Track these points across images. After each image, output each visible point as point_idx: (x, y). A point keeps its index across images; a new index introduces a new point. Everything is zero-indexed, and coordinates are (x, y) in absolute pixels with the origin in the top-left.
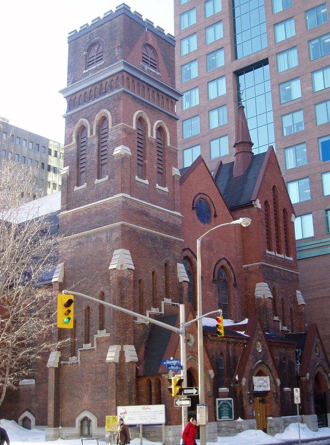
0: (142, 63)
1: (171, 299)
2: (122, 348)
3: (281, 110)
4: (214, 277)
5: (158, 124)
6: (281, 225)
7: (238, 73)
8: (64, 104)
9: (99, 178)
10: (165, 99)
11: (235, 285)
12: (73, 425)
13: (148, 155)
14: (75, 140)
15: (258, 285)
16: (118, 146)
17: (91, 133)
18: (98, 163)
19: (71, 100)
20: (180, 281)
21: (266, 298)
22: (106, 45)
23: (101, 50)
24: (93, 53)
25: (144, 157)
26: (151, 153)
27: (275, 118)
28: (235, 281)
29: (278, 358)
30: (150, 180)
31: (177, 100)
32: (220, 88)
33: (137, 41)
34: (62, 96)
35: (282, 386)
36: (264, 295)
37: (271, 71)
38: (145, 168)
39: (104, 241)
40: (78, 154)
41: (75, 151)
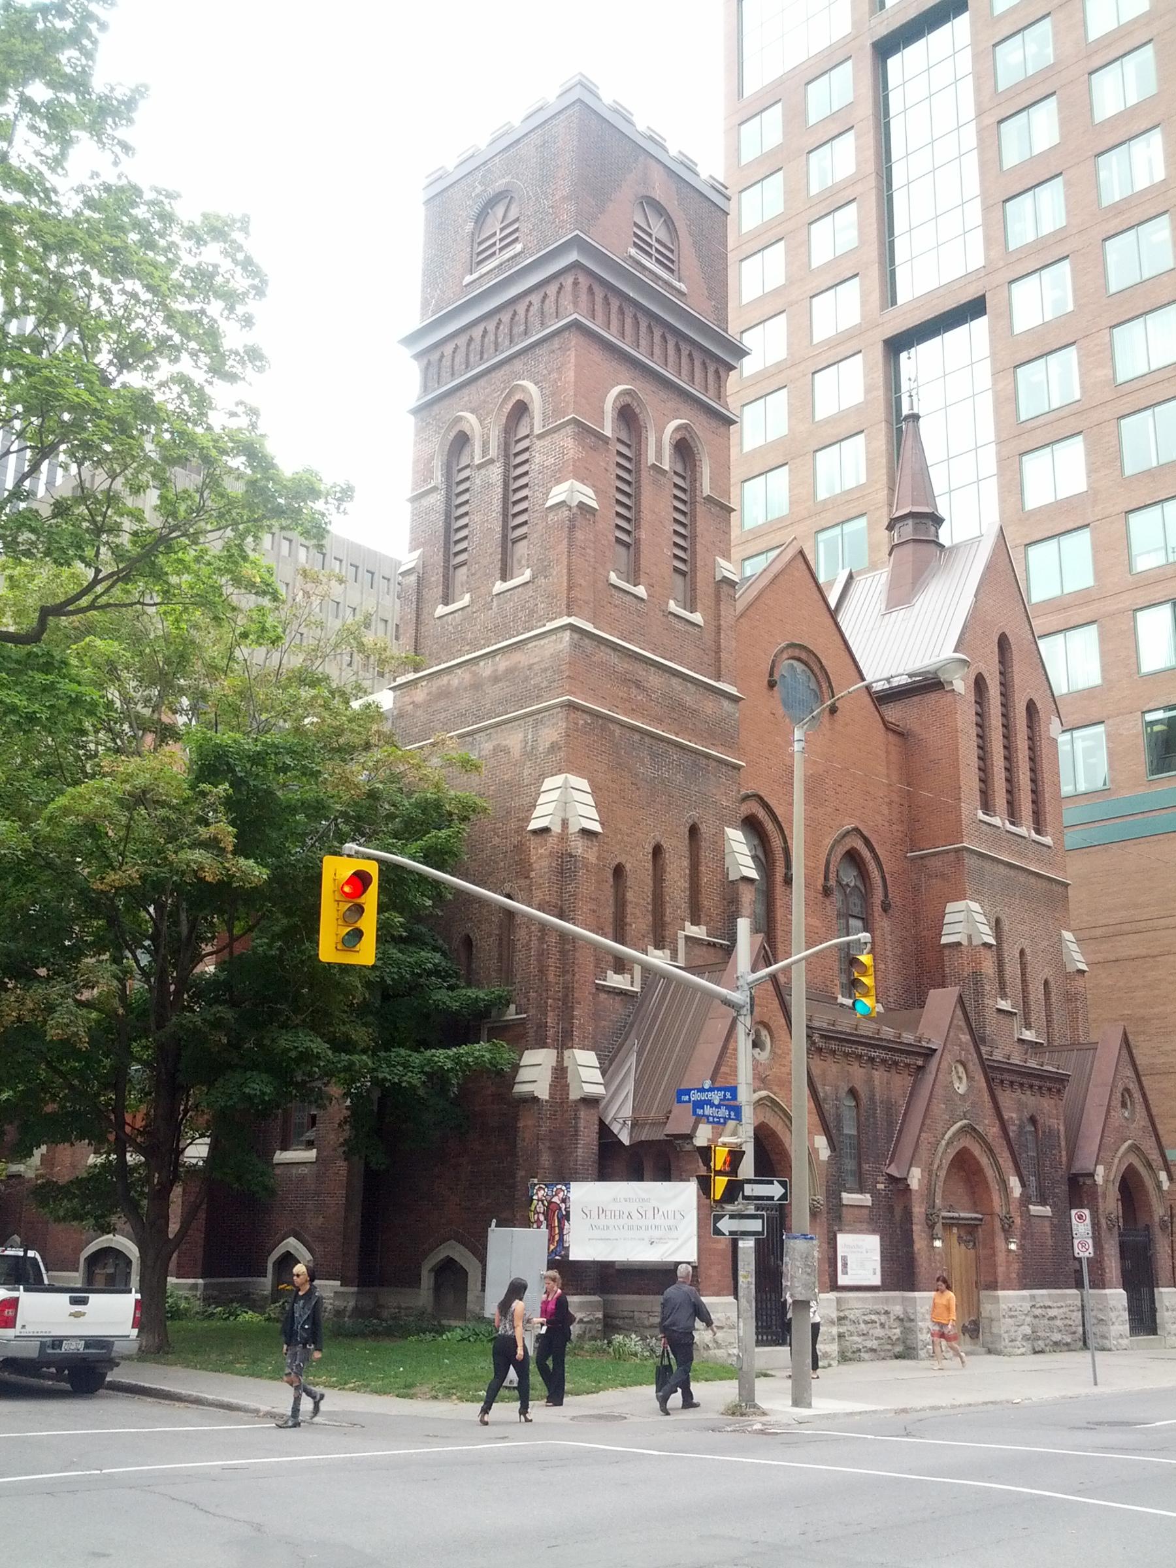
0: (633, 251)
1: (704, 928)
2: (560, 1059)
3: (1020, 439)
4: (826, 878)
5: (678, 429)
6: (1022, 744)
7: (897, 345)
8: (412, 373)
9: (504, 579)
10: (697, 363)
11: (886, 907)
12: (415, 1282)
13: (646, 515)
14: (439, 473)
15: (950, 907)
16: (558, 482)
17: (485, 451)
18: (505, 537)
19: (429, 363)
21: (974, 943)
22: (529, 198)
23: (512, 215)
24: (493, 224)
25: (635, 521)
26: (657, 506)
27: (1001, 461)
28: (886, 896)
29: (1014, 1115)
30: (650, 587)
31: (732, 368)
32: (846, 387)
33: (620, 186)
34: (407, 353)
35: (1025, 1200)
36: (970, 937)
37: (992, 331)
38: (638, 552)
39: (516, 751)
40: (448, 514)
41: (441, 507)
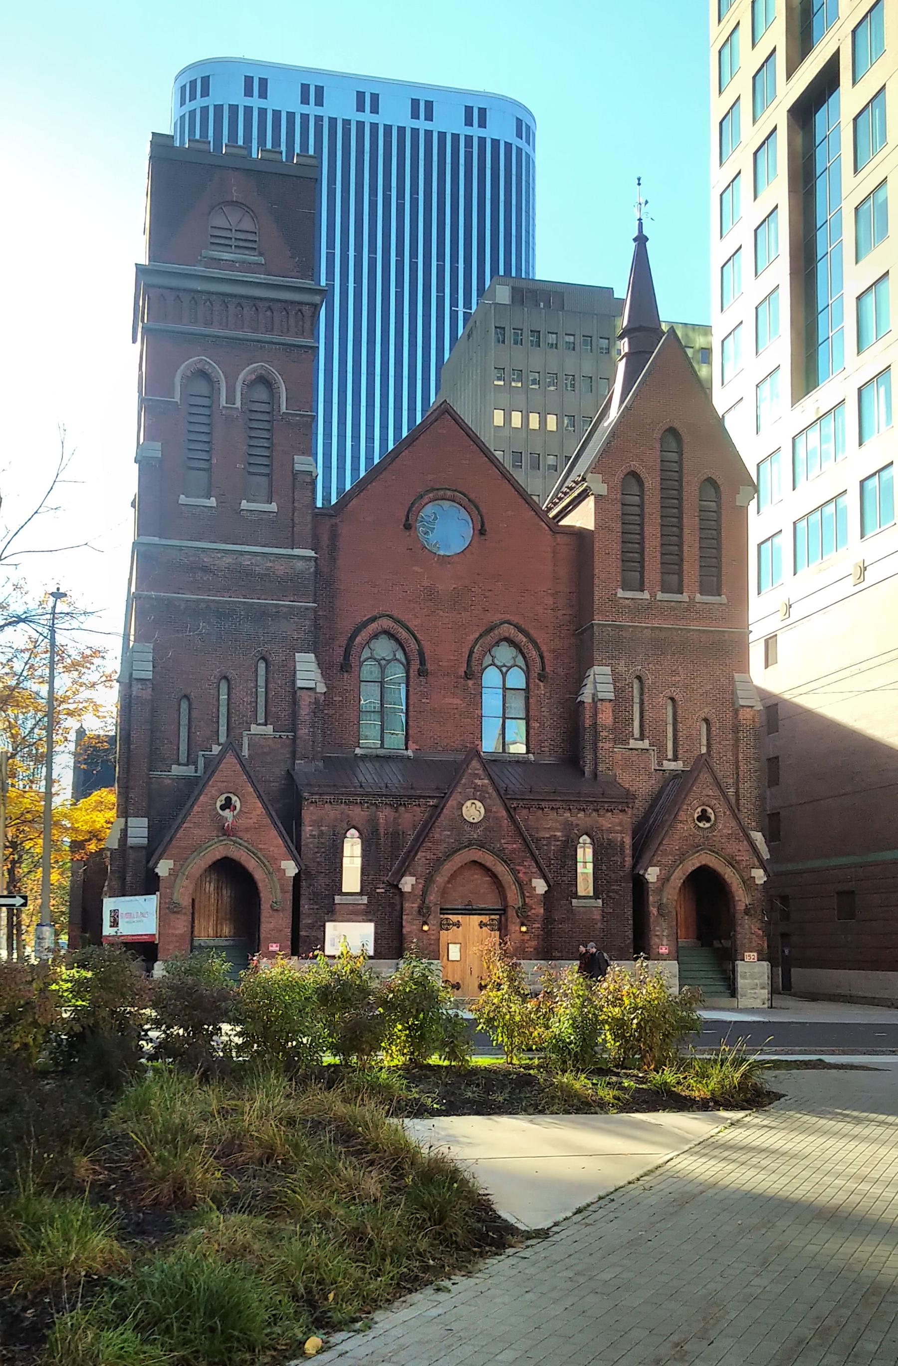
29: (559, 834)
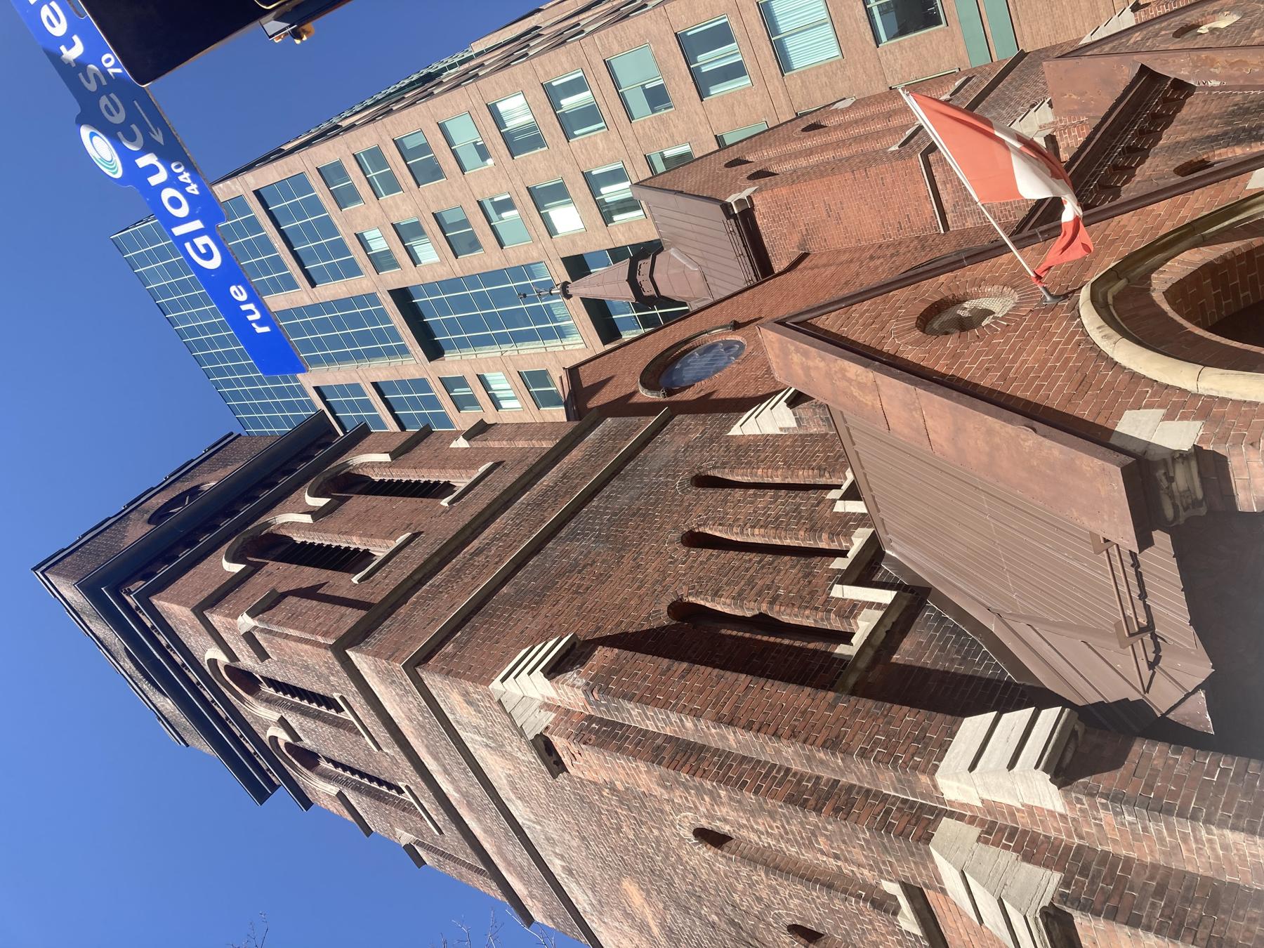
20: (794, 425)
